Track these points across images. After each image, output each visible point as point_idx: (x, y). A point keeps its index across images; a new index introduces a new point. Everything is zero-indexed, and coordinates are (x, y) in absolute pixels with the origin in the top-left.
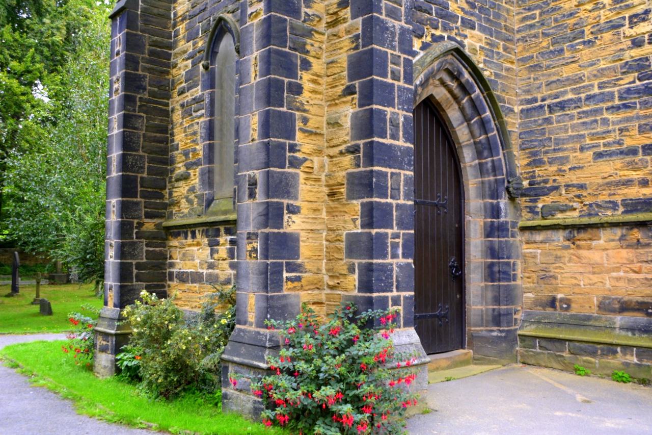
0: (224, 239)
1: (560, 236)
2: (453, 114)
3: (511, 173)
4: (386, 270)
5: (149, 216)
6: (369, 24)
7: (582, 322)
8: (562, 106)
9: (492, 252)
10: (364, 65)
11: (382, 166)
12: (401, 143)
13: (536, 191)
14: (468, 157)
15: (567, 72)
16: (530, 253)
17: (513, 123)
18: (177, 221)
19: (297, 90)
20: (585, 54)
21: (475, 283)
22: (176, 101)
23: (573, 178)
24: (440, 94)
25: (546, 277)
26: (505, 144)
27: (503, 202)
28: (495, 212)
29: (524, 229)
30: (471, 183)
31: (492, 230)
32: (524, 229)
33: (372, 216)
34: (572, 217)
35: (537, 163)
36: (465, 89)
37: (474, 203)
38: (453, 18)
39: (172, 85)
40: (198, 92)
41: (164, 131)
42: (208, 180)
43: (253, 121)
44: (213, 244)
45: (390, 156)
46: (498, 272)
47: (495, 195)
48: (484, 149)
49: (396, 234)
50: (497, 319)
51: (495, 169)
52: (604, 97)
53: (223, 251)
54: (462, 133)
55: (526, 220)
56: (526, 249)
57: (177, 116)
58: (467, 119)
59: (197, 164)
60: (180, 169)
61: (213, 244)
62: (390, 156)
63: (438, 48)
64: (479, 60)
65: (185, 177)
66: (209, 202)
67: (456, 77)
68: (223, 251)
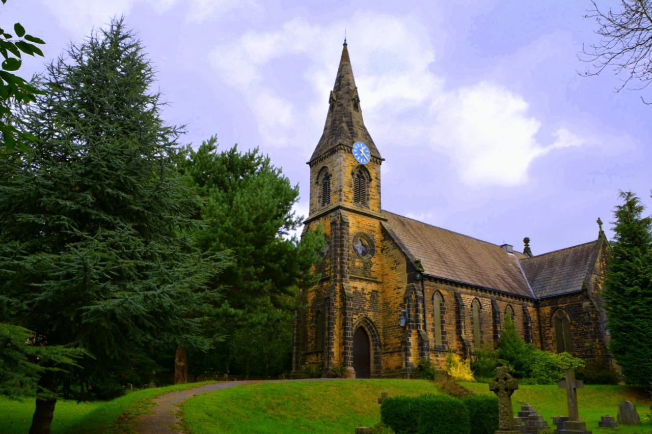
0: (320, 355)
1: (389, 354)
2: (366, 329)
3: (380, 341)
4: (348, 357)
5: (303, 350)
6: (345, 317)
7: (392, 372)
8: (389, 327)
9: (376, 358)
10: (345, 324)
11: (35, 286)
12: (351, 337)
13: (385, 345)
14: (370, 338)
15: (390, 320)
16: (384, 358)
17: (380, 331)
18: (309, 352)
19: (334, 328)
20: (393, 317)
21: (372, 365)
22: (308, 326)
23: (391, 342)
24: (363, 325)
25: (387, 364)
26: (379, 335)
27: (378, 348)
28: (376, 349)
29: (383, 353)
30: (371, 343)
31: (375, 353)
32: (383, 353)
33: (345, 348)
34: (390, 350)
35: (385, 339)
36: (369, 324)
37: (372, 348)
38: (365, 310)
39: (459, 396)
40: (314, 324)
41: (305, 332)
42: (316, 342)
43: (513, 431)
44: (317, 356)
45: (349, 339)
46: (377, 362)
47: (376, 346)
48: (373, 336)
49: (350, 352)
50: (376, 372)
51: (376, 340)
52: (396, 326)
53: (319, 357)
54: (369, 333)
55: (383, 351)
56: (383, 358)
57: (309, 329)
58: (369, 330)
59: (313, 339)
60: (309, 340)
61: (317, 356)
62: (349, 339)
63: (361, 317)
64: (372, 318)
65: (311, 342)
66: (316, 347)
67: (366, 322)
68: (319, 357)
